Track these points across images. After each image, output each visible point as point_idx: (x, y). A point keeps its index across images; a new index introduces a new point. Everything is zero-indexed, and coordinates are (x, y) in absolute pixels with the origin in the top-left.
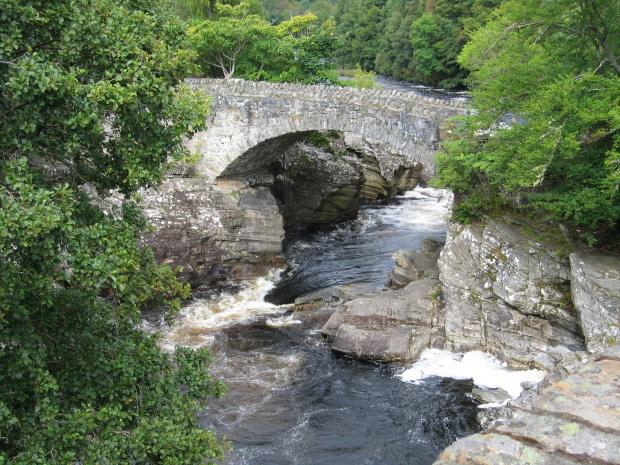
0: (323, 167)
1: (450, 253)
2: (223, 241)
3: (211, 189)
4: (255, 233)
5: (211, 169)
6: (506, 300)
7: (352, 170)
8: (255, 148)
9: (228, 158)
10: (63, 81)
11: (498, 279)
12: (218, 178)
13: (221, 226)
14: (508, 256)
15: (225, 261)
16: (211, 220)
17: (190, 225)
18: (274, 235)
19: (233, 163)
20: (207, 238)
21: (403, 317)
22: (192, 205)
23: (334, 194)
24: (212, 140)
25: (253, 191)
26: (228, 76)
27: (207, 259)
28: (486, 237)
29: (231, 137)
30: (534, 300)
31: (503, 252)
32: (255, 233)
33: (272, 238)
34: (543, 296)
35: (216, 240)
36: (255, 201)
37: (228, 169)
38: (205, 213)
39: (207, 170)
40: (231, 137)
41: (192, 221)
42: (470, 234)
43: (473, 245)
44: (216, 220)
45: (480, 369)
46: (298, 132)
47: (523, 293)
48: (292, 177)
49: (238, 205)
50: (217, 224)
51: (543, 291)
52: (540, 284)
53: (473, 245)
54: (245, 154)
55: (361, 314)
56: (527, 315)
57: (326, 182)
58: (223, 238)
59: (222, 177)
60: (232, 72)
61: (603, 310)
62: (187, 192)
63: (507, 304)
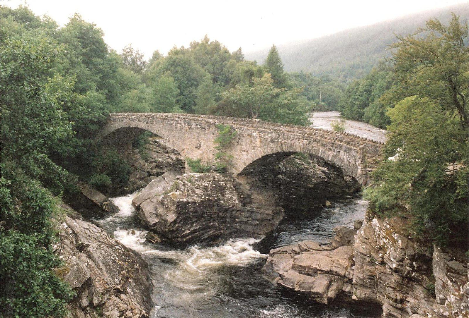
0: (307, 172)
1: (362, 232)
2: (238, 211)
3: (234, 180)
4: (258, 208)
5: (235, 169)
6: (391, 266)
7: (323, 175)
8: (260, 159)
9: (245, 163)
10: (8, 119)
11: (388, 252)
12: (238, 175)
13: (237, 202)
14: (396, 238)
15: (238, 222)
16: (232, 198)
17: (219, 200)
18: (268, 210)
19: (248, 166)
20: (229, 208)
21: (327, 269)
22: (221, 190)
23: (311, 188)
24: (237, 153)
25: (259, 183)
26: (254, 117)
27: (228, 220)
28: (385, 225)
29: (247, 151)
30: (408, 268)
31: (393, 236)
32: (258, 208)
33: (267, 212)
34: (414, 266)
35: (233, 210)
36: (260, 190)
37: (245, 169)
38: (228, 193)
39: (233, 169)
40: (247, 151)
41: (221, 197)
42: (263, 238)
43: (377, 228)
44: (235, 198)
45: (438, 299)
46: (284, 152)
47: (401, 263)
48: (288, 177)
49: (249, 190)
50: (235, 200)
51: (414, 263)
52: (413, 258)
53: (377, 228)
54: (255, 162)
55: (303, 264)
56: (403, 277)
57: (308, 181)
58: (238, 209)
59: (242, 174)
60: (257, 116)
61: (449, 282)
62: (220, 181)
63: (391, 269)
